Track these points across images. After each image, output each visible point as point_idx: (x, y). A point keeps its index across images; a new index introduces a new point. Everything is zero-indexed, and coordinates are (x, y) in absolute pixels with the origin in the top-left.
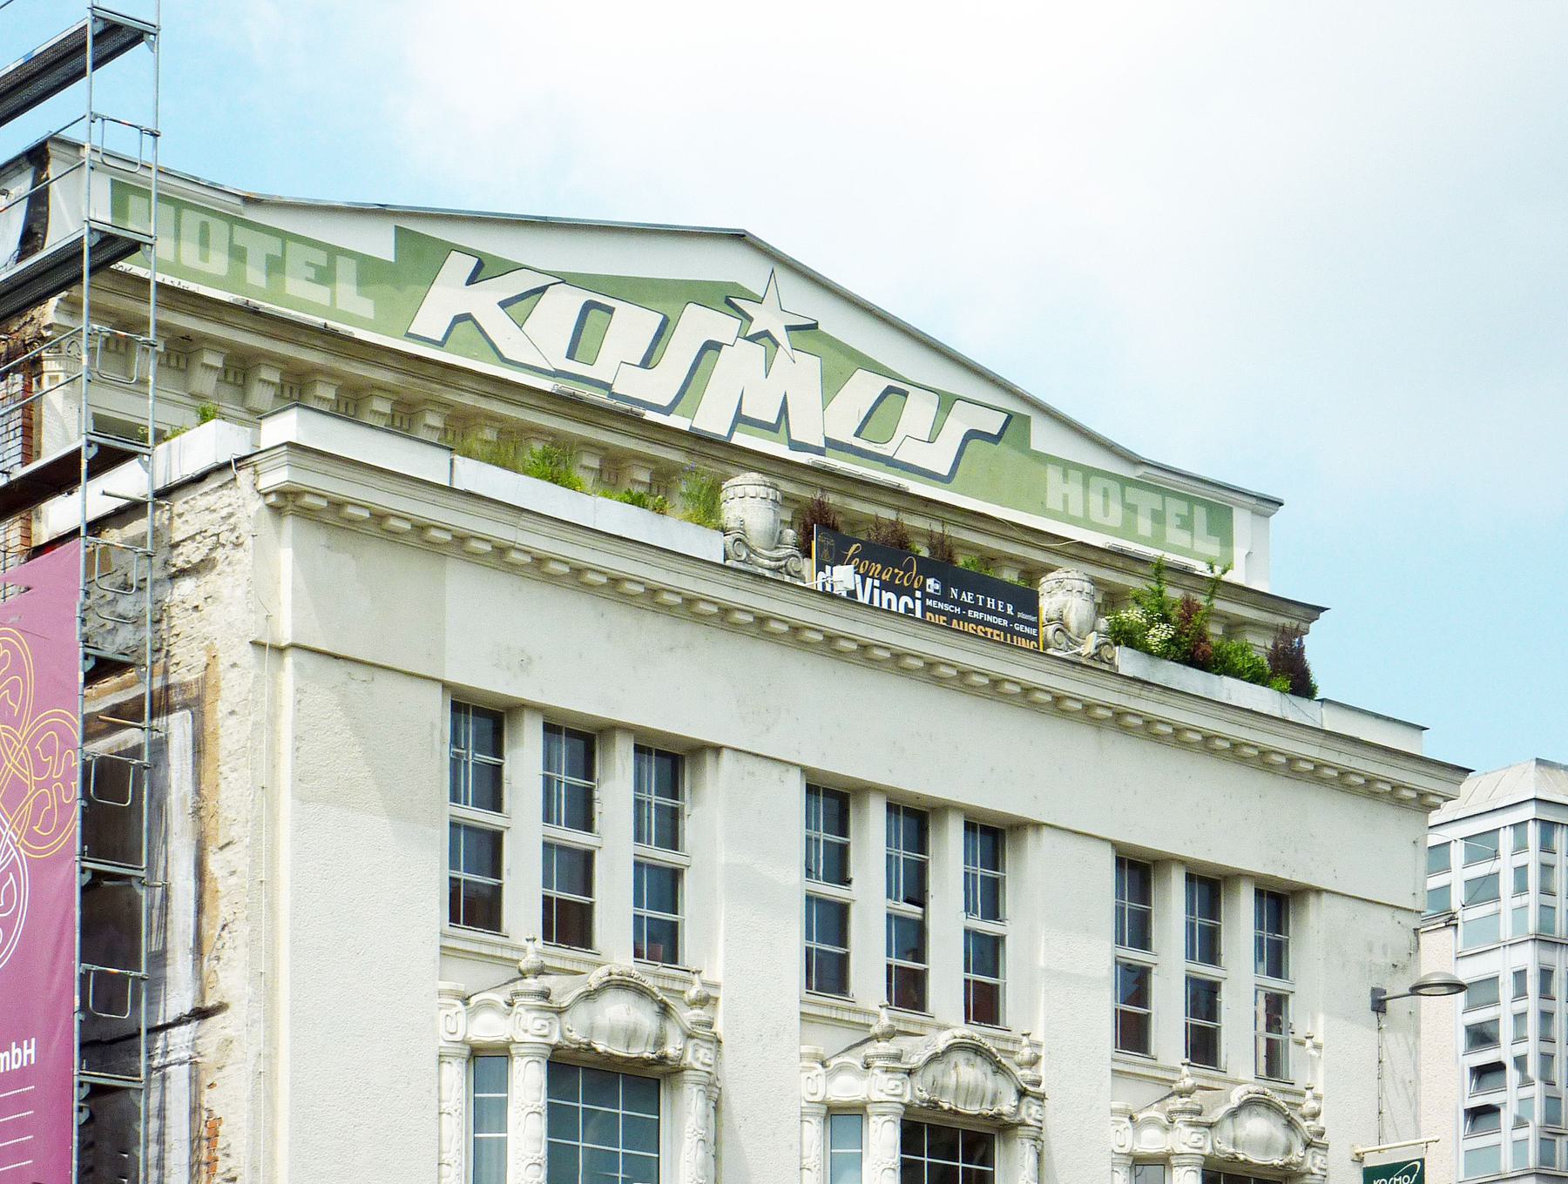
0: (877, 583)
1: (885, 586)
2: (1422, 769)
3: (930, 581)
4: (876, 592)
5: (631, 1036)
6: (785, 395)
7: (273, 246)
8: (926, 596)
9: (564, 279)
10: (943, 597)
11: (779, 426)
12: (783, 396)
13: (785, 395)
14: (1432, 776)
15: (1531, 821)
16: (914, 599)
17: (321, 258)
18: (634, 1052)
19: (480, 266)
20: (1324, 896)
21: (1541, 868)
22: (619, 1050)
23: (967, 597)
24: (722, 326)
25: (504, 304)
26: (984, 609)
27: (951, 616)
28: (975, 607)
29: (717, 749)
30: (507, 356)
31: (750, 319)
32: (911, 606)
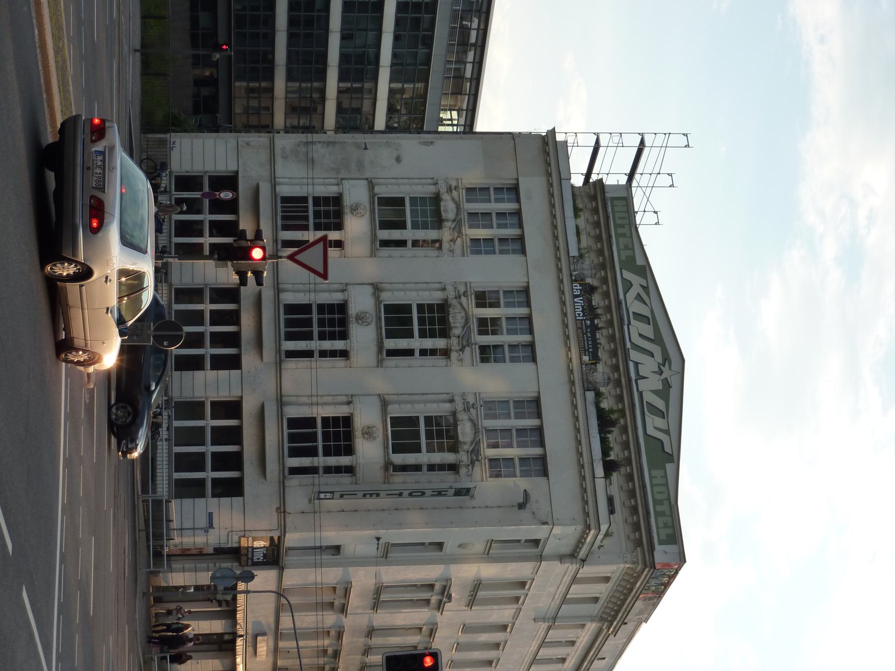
0: (583, 304)
1: (583, 307)
2: (596, 517)
3: (589, 322)
4: (580, 304)
5: (446, 211)
6: (647, 378)
7: (628, 234)
8: (585, 320)
9: (652, 311)
10: (587, 327)
11: (640, 377)
12: (646, 376)
13: (647, 378)
14: (594, 515)
15: (526, 280)
16: (583, 316)
17: (630, 246)
18: (442, 213)
19: (646, 288)
20: (547, 481)
21: (494, 190)
22: (442, 209)
23: (589, 334)
24: (659, 358)
25: (638, 294)
26: (588, 341)
27: (581, 328)
28: (587, 337)
29: (526, 256)
30: (627, 295)
31: (664, 366)
32: (581, 316)
